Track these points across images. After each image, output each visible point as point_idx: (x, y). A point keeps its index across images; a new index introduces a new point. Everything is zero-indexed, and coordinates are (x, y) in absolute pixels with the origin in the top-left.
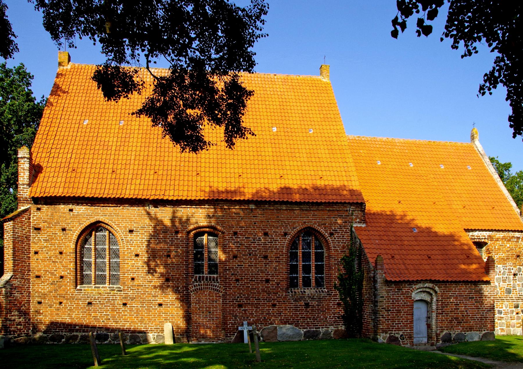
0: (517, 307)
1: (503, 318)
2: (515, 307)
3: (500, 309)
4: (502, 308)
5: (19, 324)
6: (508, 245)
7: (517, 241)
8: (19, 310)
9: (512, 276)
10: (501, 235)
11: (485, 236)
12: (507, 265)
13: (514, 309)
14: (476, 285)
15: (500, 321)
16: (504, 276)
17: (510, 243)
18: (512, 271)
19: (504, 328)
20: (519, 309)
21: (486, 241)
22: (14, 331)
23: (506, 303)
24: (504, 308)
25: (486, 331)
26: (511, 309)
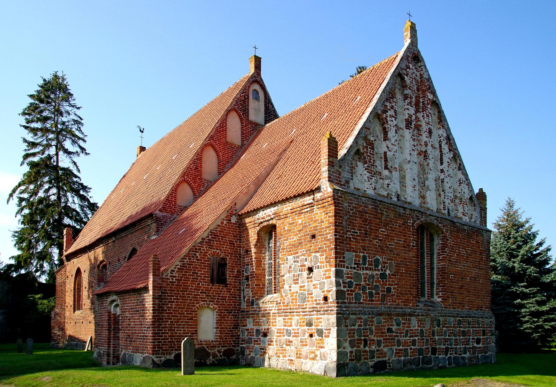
0: (310, 324)
1: (291, 342)
2: (307, 326)
3: (289, 328)
4: (291, 326)
5: (59, 336)
6: (300, 221)
7: (312, 211)
8: (59, 327)
9: (305, 273)
10: (287, 207)
11: (269, 216)
12: (300, 254)
13: (306, 328)
14: (140, 294)
15: (288, 347)
16: (296, 274)
17: (303, 216)
18: (306, 263)
19: (294, 359)
20: (313, 327)
21: (274, 222)
22: (56, 340)
23: (296, 317)
24: (294, 327)
25: (146, 355)
26: (302, 328)
